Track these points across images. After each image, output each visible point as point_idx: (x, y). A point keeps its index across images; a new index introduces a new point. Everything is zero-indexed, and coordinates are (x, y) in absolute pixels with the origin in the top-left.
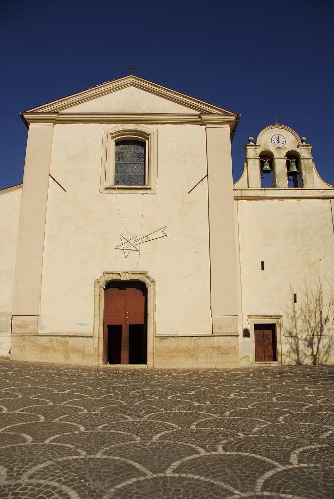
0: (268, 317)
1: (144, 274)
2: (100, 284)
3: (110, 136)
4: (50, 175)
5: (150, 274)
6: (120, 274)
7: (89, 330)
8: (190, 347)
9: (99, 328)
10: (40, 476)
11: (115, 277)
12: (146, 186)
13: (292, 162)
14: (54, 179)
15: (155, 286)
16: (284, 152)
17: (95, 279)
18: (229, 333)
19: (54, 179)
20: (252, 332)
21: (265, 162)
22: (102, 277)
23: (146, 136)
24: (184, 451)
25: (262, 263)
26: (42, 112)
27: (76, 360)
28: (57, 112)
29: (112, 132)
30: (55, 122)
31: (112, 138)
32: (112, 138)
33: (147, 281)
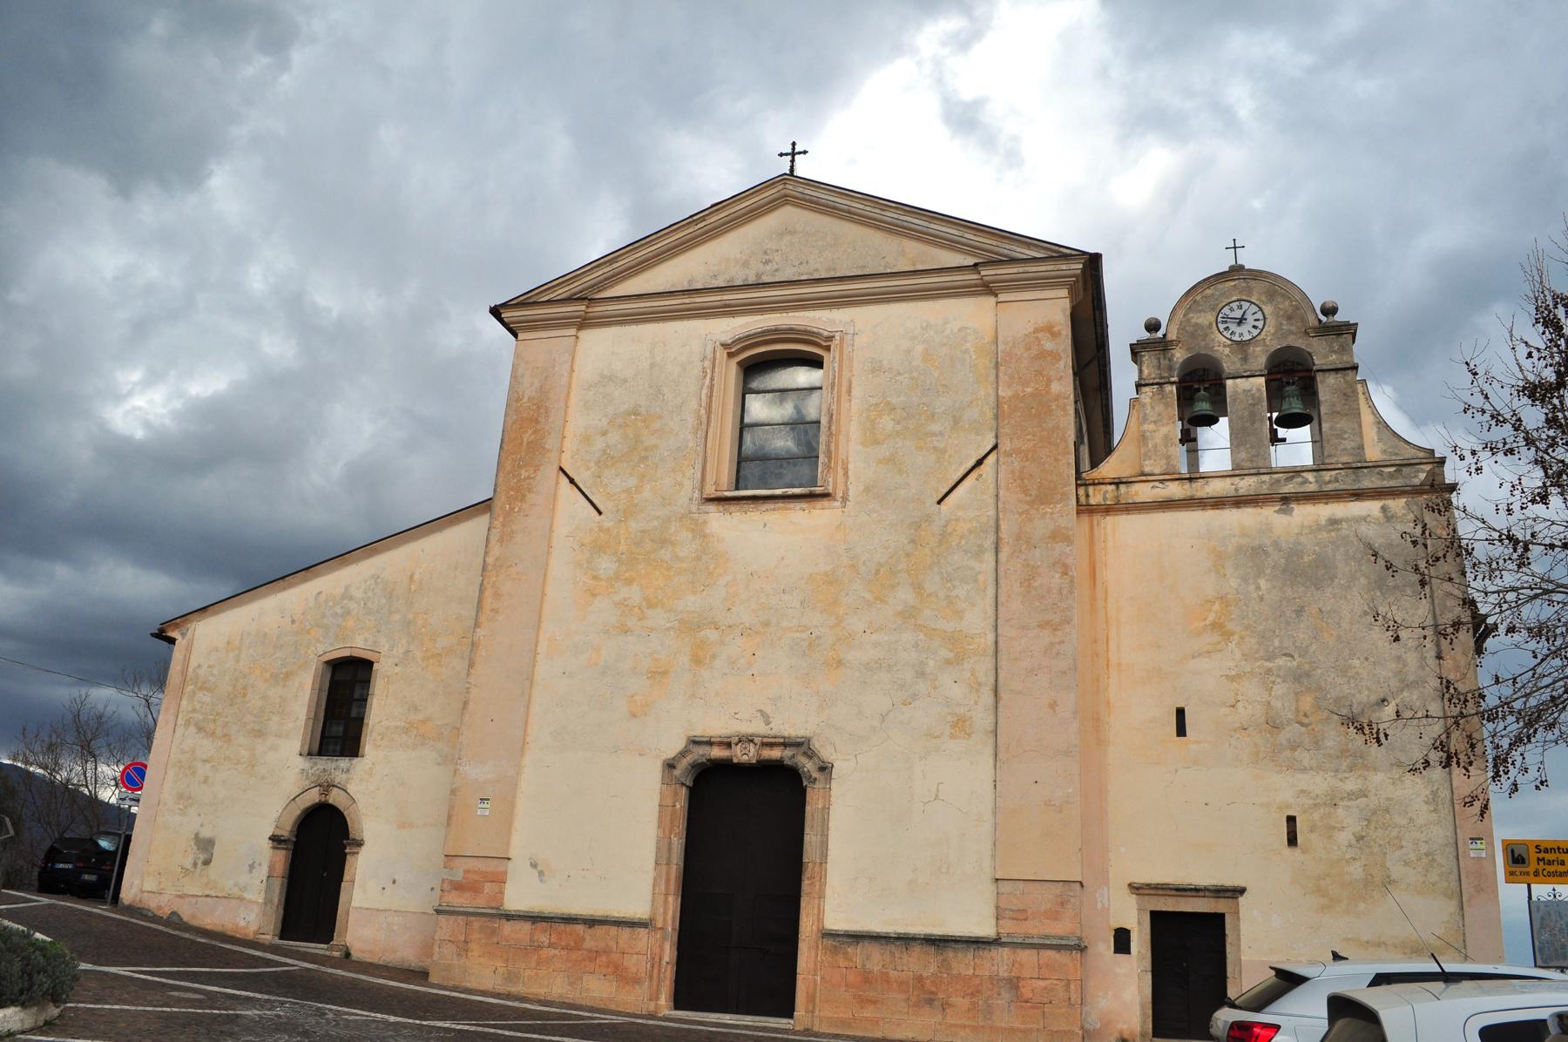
0: (1196, 891)
1: (801, 745)
2: (677, 772)
3: (722, 354)
4: (561, 469)
5: (816, 745)
6: (729, 745)
7: (637, 905)
8: (925, 974)
9: (666, 902)
10: (1528, 270)
11: (717, 753)
12: (818, 490)
13: (1288, 384)
14: (572, 481)
15: (829, 779)
16: (1260, 360)
17: (664, 757)
18: (1047, 937)
19: (572, 481)
20: (1140, 942)
21: (1199, 390)
22: (683, 754)
23: (826, 342)
24: (831, 484)
25: (1180, 713)
26: (548, 301)
27: (597, 990)
28: (585, 299)
29: (728, 339)
30: (584, 323)
31: (730, 355)
32: (730, 355)
33: (808, 766)
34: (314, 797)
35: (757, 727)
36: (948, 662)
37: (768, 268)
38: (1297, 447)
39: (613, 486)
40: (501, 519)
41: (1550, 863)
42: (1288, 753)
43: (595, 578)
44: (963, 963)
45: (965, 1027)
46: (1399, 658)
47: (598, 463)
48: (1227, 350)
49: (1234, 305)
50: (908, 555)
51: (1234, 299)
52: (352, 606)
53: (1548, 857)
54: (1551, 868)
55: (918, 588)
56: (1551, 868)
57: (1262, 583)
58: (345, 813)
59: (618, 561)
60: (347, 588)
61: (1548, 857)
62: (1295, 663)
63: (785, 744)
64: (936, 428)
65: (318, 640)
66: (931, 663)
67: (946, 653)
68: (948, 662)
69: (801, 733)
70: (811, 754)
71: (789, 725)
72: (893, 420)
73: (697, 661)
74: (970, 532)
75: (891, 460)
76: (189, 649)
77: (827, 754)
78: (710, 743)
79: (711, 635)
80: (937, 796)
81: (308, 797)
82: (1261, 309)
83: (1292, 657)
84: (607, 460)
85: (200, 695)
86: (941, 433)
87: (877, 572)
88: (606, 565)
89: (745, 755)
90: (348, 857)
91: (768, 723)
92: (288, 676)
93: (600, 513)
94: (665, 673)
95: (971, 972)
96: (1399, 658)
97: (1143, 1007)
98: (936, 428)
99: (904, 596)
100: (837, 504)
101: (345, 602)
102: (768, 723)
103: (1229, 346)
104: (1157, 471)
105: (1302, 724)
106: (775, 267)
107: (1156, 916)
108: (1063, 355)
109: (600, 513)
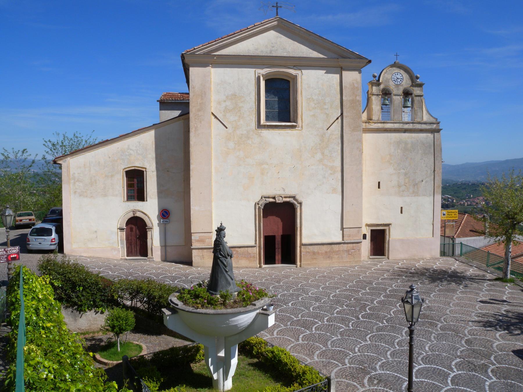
5: (297, 197)
34: (131, 215)
35: (281, 192)
36: (331, 174)
37: (274, 49)
38: (406, 116)
39: (230, 119)
40: (194, 129)
41: (450, 215)
42: (402, 192)
43: (228, 149)
44: (336, 247)
45: (337, 262)
46: (426, 170)
47: (224, 111)
48: (394, 86)
49: (396, 74)
50: (320, 144)
51: (396, 71)
52: (131, 152)
53: (450, 214)
54: (450, 216)
55: (323, 154)
56: (450, 216)
57: (399, 151)
58: (144, 219)
59: (235, 143)
60: (129, 146)
61: (450, 214)
62: (405, 171)
63: (290, 197)
64: (326, 107)
65: (121, 164)
66: (327, 174)
67: (330, 172)
68: (331, 174)
69: (294, 193)
70: (296, 200)
71: (290, 192)
72: (314, 103)
73: (262, 174)
74: (336, 138)
75: (314, 115)
76: (68, 167)
77: (300, 199)
78: (269, 197)
79: (265, 166)
80: (329, 208)
81: (203, 245)
82: (402, 76)
83: (404, 169)
84: (226, 110)
85: (77, 183)
86: (328, 109)
87: (312, 149)
88: (231, 145)
89: (279, 200)
90: (148, 232)
91: (284, 191)
92: (112, 176)
93: (227, 128)
94: (253, 178)
95: (338, 250)
96: (426, 170)
97: (368, 250)
98: (326, 107)
99: (319, 156)
100: (300, 128)
101: (129, 151)
102: (284, 191)
103: (394, 85)
104: (376, 119)
105: (405, 186)
106: (276, 49)
107: (372, 231)
108: (360, 89)
109: (227, 128)
